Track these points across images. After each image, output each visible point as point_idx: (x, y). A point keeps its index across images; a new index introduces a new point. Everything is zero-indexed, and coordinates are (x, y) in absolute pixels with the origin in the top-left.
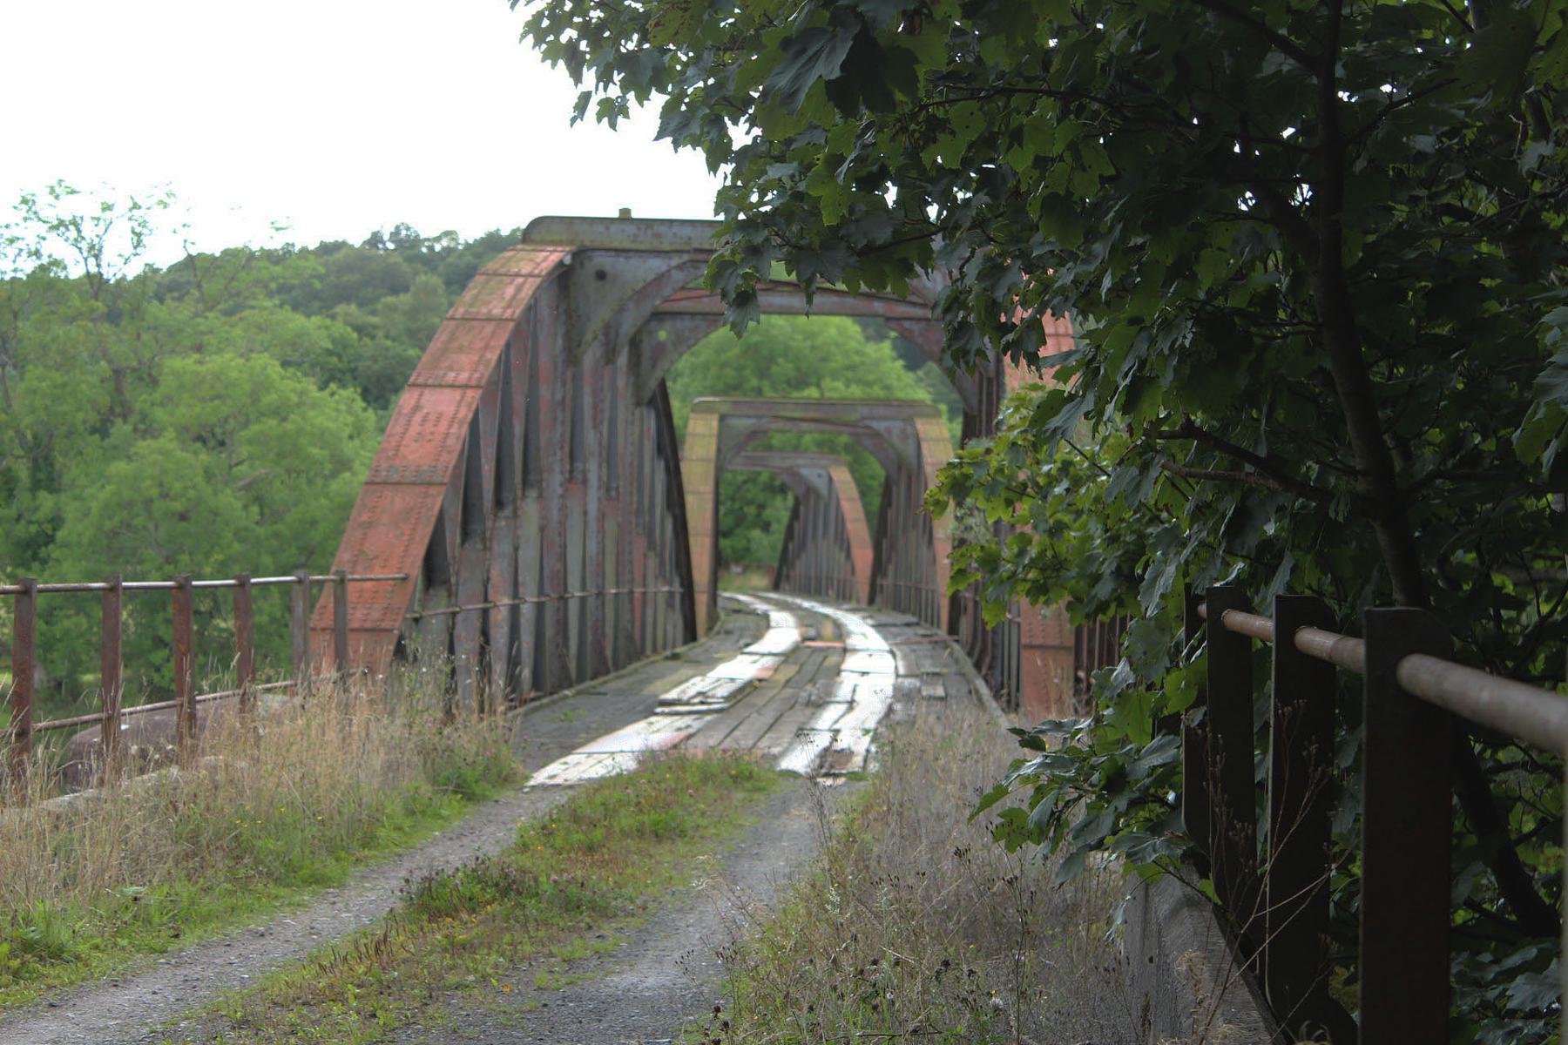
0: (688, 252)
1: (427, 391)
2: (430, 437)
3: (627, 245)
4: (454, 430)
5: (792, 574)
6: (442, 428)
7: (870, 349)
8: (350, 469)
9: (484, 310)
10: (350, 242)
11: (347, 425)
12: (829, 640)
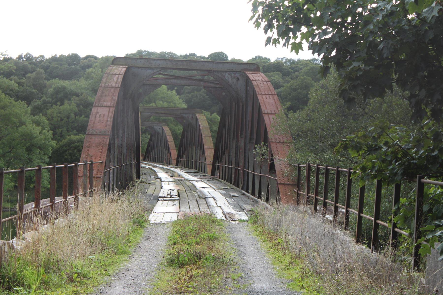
0: (159, 68)
1: (99, 108)
2: (102, 121)
3: (142, 66)
4: (109, 119)
5: (149, 156)
6: (106, 118)
7: (169, 92)
8: (25, 124)
9: (110, 85)
10: (13, 58)
11: (23, 112)
12: (176, 177)
